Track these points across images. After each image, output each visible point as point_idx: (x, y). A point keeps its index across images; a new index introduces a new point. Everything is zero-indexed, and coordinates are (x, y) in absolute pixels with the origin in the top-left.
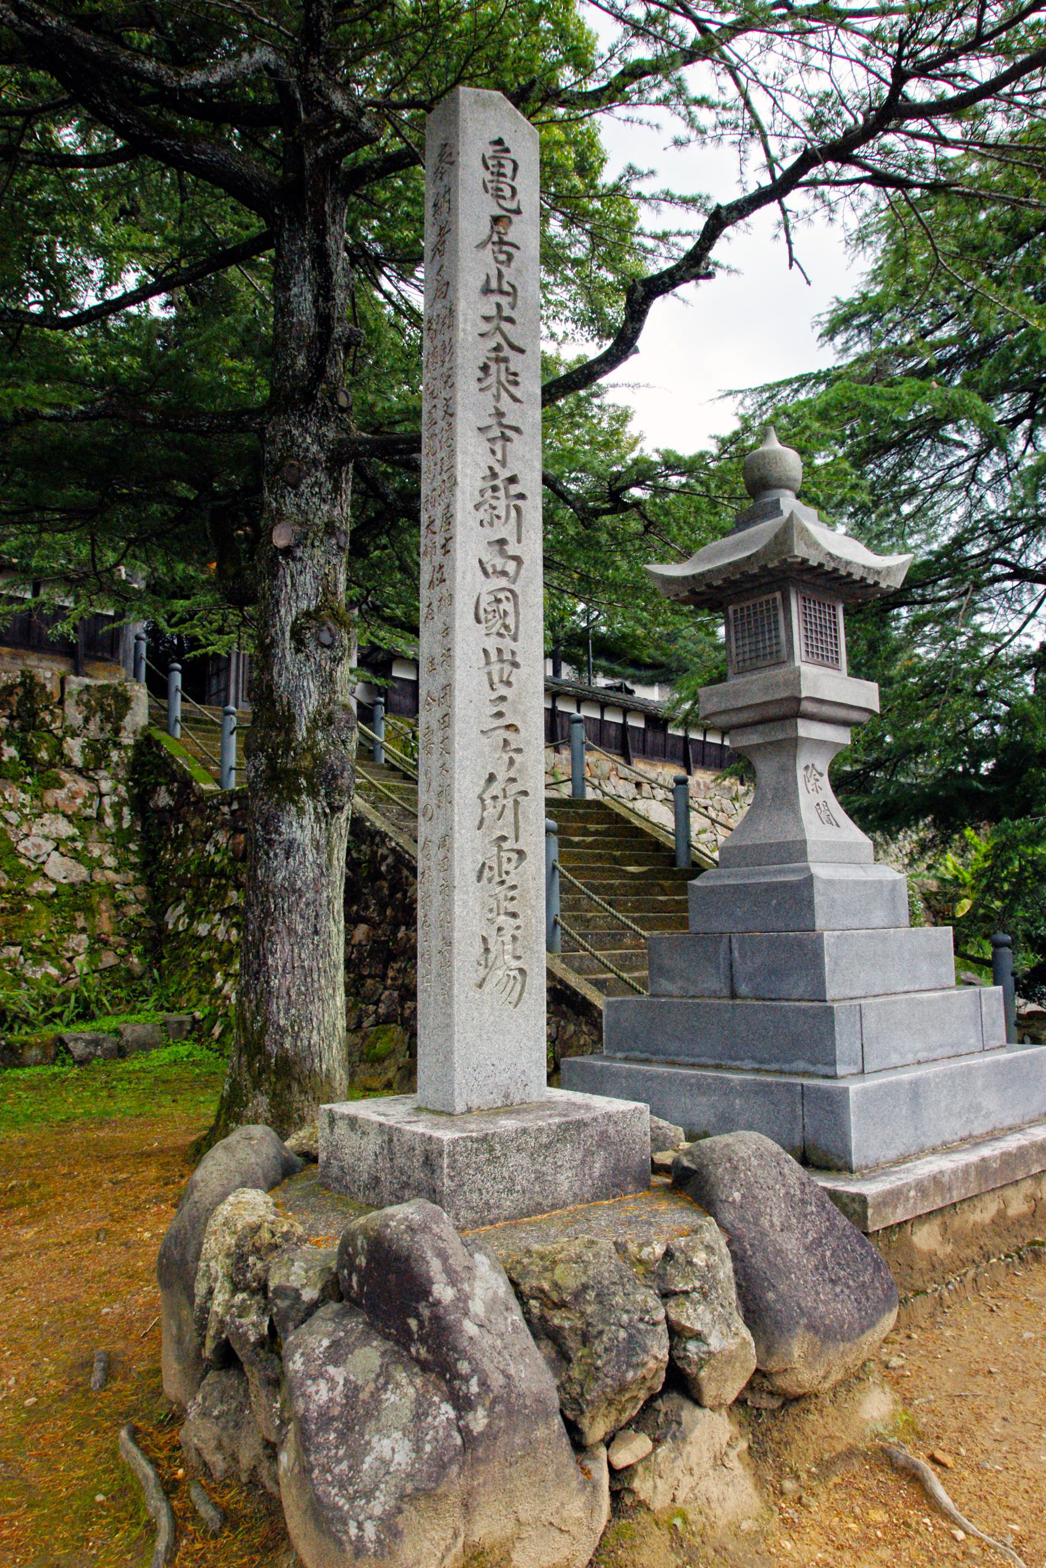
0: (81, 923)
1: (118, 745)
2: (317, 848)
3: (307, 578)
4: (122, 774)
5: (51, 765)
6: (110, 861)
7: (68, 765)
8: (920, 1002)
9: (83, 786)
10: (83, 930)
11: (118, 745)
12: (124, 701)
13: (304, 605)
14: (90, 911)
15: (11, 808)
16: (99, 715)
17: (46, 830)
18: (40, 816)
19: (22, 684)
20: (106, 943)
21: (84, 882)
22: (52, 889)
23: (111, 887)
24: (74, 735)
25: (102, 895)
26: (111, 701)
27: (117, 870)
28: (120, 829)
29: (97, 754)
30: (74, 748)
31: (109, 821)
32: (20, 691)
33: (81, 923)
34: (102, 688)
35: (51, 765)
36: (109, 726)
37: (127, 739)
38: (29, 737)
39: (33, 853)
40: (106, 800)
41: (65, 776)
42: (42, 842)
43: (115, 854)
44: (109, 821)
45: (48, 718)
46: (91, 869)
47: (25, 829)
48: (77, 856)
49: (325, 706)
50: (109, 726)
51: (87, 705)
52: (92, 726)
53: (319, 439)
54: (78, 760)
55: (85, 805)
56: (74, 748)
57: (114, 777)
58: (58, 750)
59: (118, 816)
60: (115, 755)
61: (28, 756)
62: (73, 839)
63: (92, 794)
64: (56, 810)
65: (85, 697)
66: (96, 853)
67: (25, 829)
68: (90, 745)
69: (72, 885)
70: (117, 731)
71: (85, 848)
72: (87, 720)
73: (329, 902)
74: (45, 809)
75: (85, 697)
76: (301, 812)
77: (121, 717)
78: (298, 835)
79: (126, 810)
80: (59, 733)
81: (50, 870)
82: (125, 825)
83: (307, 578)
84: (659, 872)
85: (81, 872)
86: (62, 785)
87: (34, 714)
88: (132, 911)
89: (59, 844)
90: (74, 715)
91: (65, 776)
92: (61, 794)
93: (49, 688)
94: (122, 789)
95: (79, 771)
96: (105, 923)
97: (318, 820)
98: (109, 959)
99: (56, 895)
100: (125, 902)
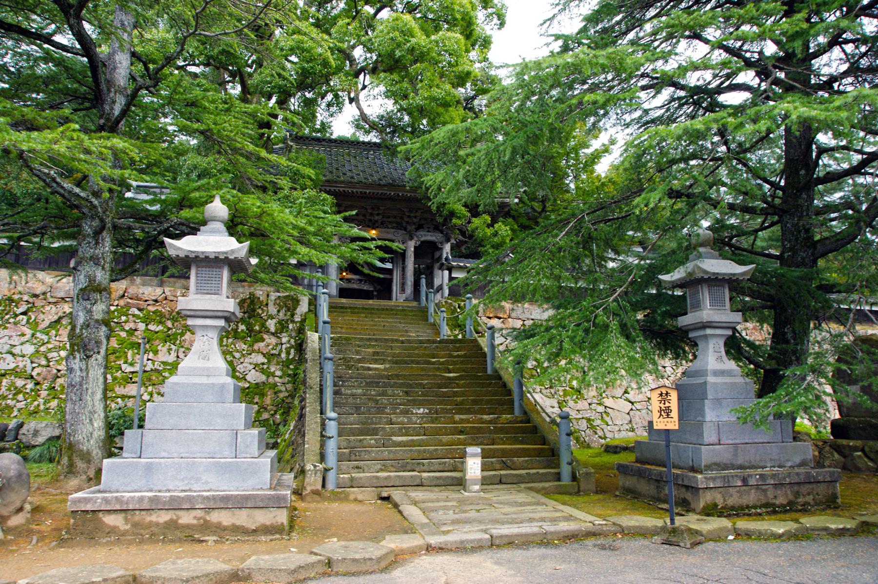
0: (256, 400)
1: (293, 322)
2: (81, 370)
3: (82, 277)
4: (294, 334)
5: (260, 332)
6: (278, 373)
7: (268, 331)
8: (188, 434)
9: (273, 340)
10: (257, 403)
11: (293, 322)
12: (296, 302)
13: (80, 286)
14: (263, 395)
15: (238, 351)
16: (284, 309)
17: (251, 361)
18: (250, 354)
19: (250, 298)
20: (266, 409)
21: (263, 383)
22: (247, 385)
23: (275, 385)
24: (272, 318)
25: (270, 388)
26: (290, 302)
27: (281, 377)
28: (288, 359)
29: (282, 327)
30: (272, 325)
31: (283, 355)
32: (248, 301)
33: (256, 400)
34: (285, 297)
35: (260, 332)
36: (289, 313)
37: (297, 318)
38: (251, 320)
39: (242, 371)
40: (284, 346)
41: (265, 336)
42: (248, 365)
43: (282, 370)
44: (283, 355)
45: (260, 312)
46: (268, 377)
47: (242, 360)
48: (263, 371)
49: (87, 320)
50: (289, 313)
51: (279, 305)
52: (281, 314)
53: (90, 226)
54: (273, 329)
55: (273, 349)
56: (272, 325)
57: (291, 336)
58: (263, 325)
59: (288, 353)
60: (291, 326)
61: (250, 330)
62: (263, 364)
63: (277, 344)
64: (259, 351)
65: (278, 302)
66: (273, 369)
67: (242, 360)
68: (280, 322)
69: (257, 384)
70: (293, 315)
71: (268, 368)
72: (279, 311)
73: (87, 389)
74: (254, 351)
75: (278, 302)
76: (75, 358)
77: (295, 309)
78: (74, 366)
79: (292, 350)
80: (265, 318)
81: (248, 378)
82: (291, 357)
83: (82, 277)
84: (469, 384)
85: (263, 378)
86: (263, 340)
87: (254, 310)
88: (281, 395)
89: (256, 366)
90: (272, 310)
91: (265, 336)
92: (262, 345)
93: (261, 299)
94: (292, 341)
95: (273, 334)
96: (268, 400)
97: (81, 360)
98: (265, 416)
99: (248, 388)
100: (281, 391)
